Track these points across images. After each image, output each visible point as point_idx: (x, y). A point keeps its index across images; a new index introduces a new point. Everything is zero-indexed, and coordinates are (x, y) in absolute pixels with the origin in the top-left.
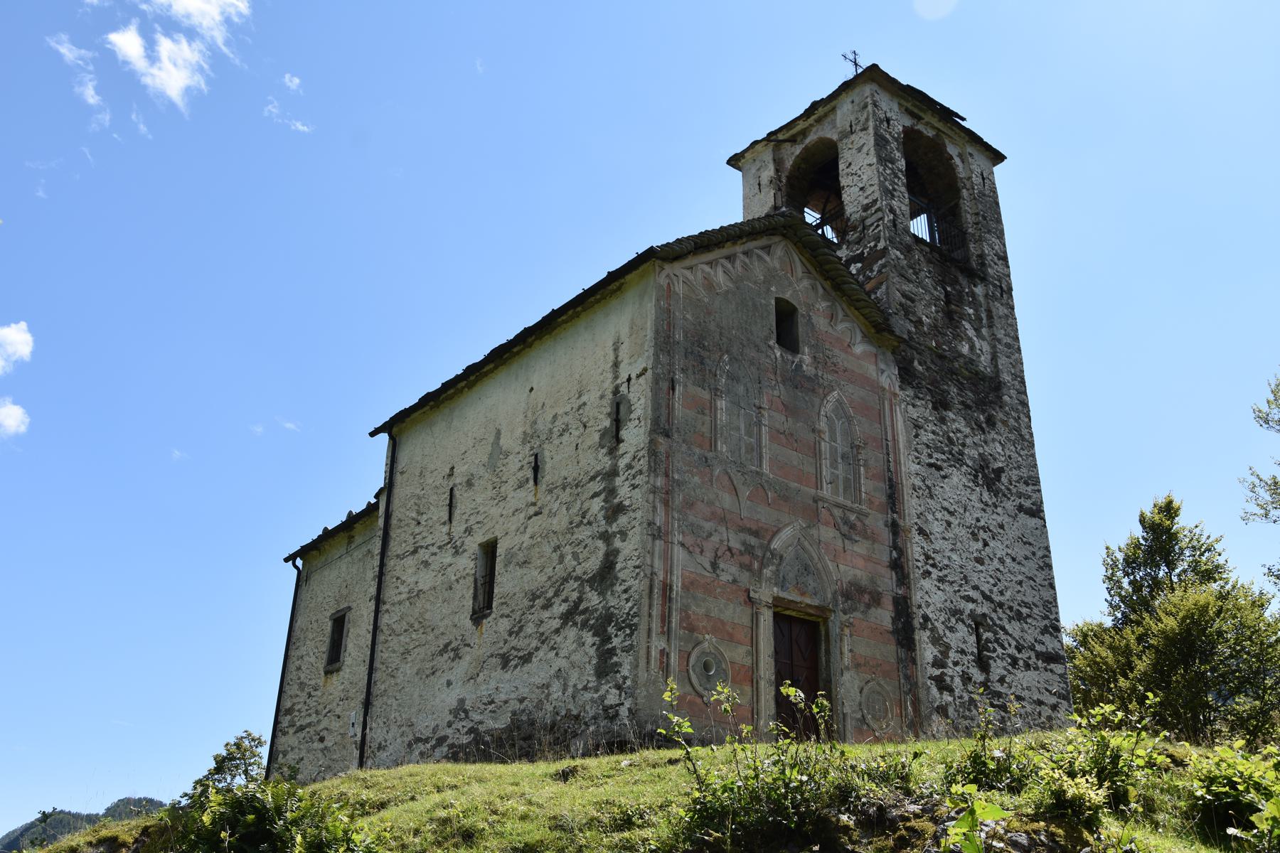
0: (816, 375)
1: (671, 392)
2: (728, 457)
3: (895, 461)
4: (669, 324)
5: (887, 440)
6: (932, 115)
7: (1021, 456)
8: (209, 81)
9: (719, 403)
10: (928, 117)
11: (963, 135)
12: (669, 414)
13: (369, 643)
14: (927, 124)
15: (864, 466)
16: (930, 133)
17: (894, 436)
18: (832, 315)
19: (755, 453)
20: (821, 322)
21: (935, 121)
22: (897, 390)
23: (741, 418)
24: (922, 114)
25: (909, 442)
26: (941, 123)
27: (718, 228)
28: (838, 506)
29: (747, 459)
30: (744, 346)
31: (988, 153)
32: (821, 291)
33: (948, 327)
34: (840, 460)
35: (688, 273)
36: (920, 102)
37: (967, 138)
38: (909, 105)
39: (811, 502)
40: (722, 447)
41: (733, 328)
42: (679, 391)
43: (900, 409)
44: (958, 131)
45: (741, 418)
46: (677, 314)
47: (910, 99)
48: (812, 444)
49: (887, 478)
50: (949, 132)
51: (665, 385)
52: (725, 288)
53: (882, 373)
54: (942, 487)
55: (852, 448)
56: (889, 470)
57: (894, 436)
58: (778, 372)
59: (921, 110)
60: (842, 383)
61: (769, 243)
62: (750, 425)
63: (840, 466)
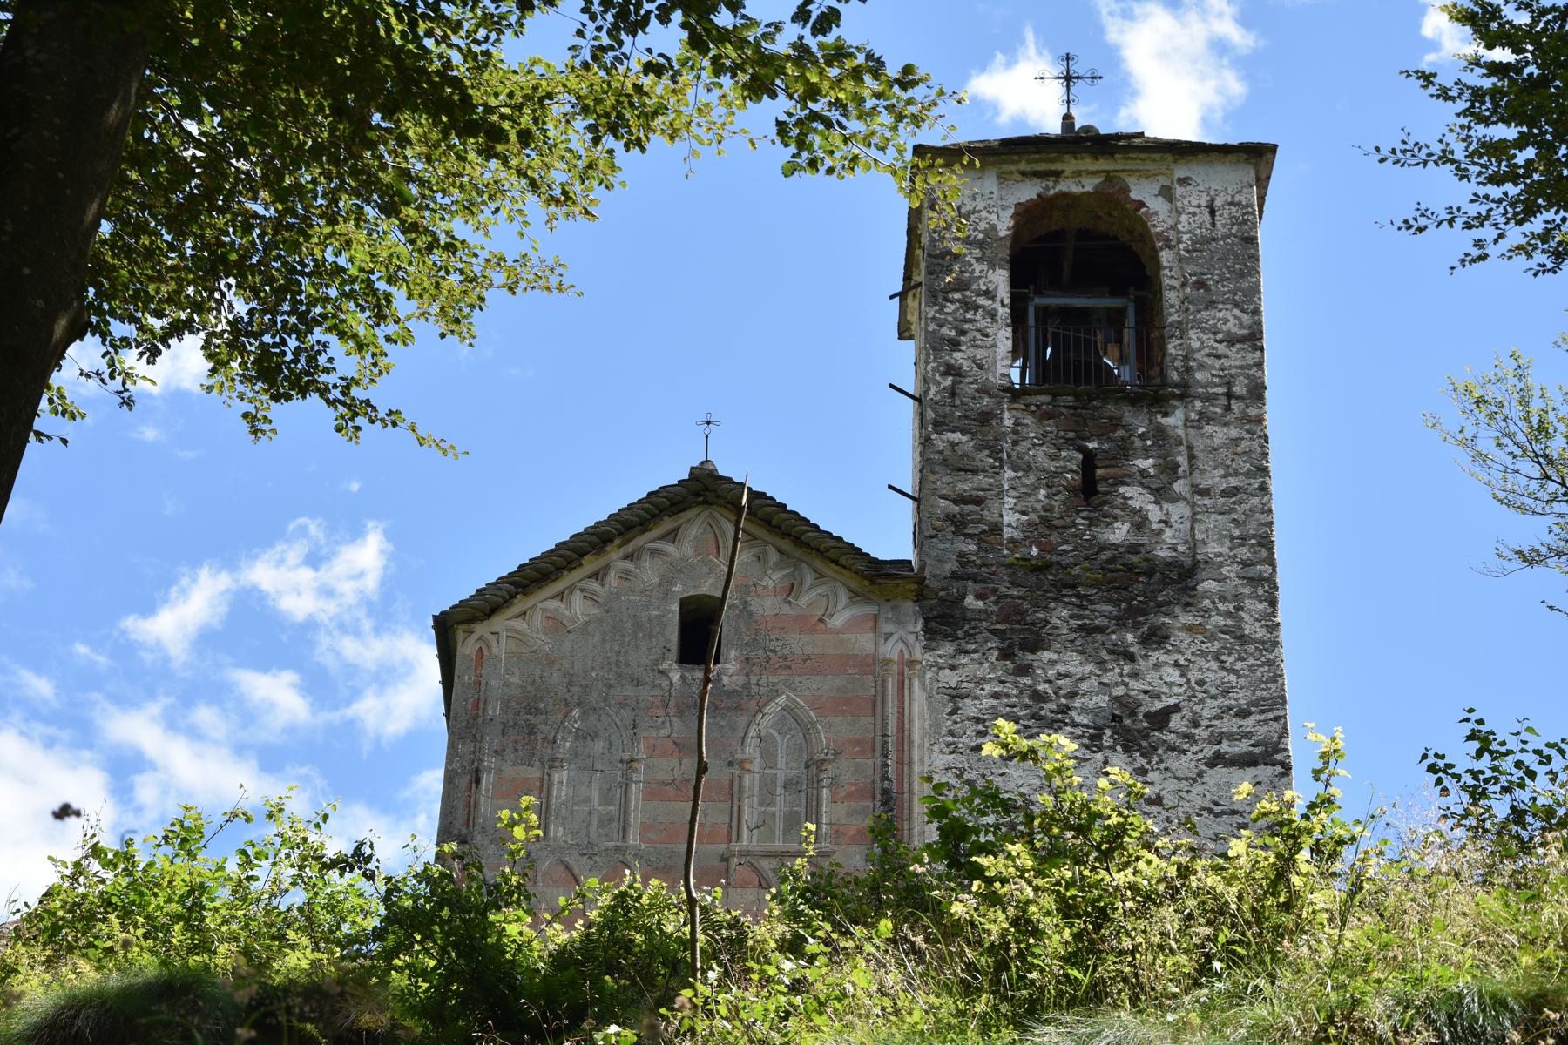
0: (747, 685)
1: (474, 785)
2: (565, 842)
3: (900, 762)
4: (808, 545)
5: (885, 735)
6: (1076, 158)
7: (1236, 672)
8: (1247, 65)
9: (556, 777)
10: (1069, 165)
11: (1157, 156)
12: (469, 815)
13: (689, 818)
14: (1078, 174)
15: (829, 786)
16: (1089, 185)
17: (901, 729)
18: (793, 585)
19: (615, 824)
20: (767, 605)
21: (1088, 164)
22: (918, 653)
23: (595, 786)
24: (1058, 167)
25: (936, 725)
26: (1101, 161)
27: (722, 472)
28: (769, 855)
29: (600, 836)
30: (610, 687)
31: (1230, 156)
32: (774, 556)
33: (1078, 512)
34: (779, 790)
35: (519, 624)
36: (1037, 153)
37: (1169, 157)
38: (1023, 166)
39: (717, 863)
40: (556, 832)
41: (593, 668)
42: (488, 780)
43: (923, 684)
44: (1142, 156)
45: (595, 786)
46: (493, 683)
47: (1015, 157)
48: (726, 784)
49: (878, 793)
50: (1130, 165)
51: (463, 781)
52: (582, 619)
53: (886, 640)
54: (1003, 774)
55: (807, 767)
56: (885, 778)
57: (901, 729)
58: (672, 702)
59: (1052, 161)
60: (797, 679)
61: (676, 524)
62: (609, 790)
63: (780, 800)
